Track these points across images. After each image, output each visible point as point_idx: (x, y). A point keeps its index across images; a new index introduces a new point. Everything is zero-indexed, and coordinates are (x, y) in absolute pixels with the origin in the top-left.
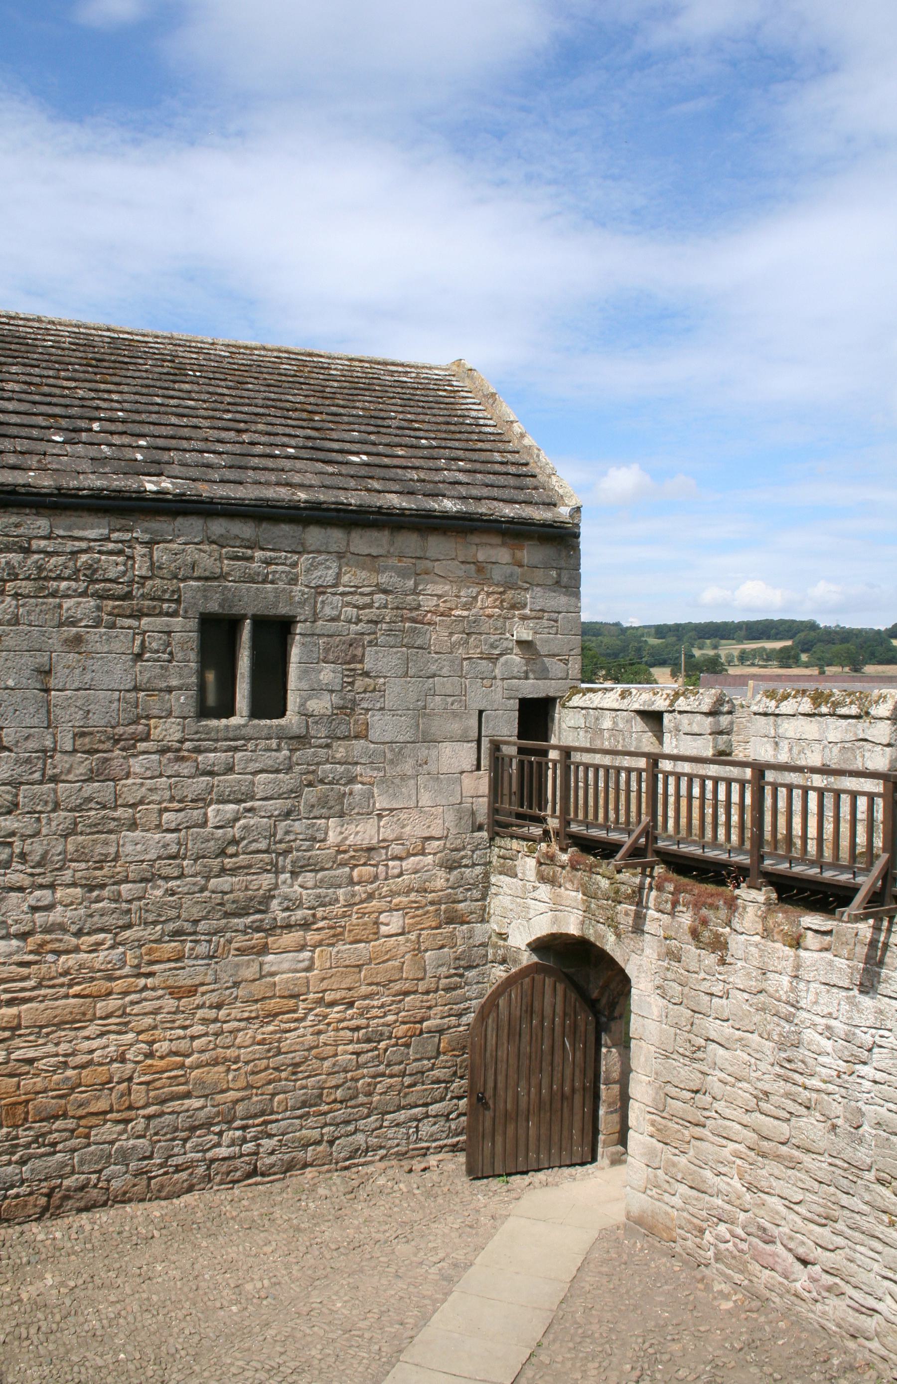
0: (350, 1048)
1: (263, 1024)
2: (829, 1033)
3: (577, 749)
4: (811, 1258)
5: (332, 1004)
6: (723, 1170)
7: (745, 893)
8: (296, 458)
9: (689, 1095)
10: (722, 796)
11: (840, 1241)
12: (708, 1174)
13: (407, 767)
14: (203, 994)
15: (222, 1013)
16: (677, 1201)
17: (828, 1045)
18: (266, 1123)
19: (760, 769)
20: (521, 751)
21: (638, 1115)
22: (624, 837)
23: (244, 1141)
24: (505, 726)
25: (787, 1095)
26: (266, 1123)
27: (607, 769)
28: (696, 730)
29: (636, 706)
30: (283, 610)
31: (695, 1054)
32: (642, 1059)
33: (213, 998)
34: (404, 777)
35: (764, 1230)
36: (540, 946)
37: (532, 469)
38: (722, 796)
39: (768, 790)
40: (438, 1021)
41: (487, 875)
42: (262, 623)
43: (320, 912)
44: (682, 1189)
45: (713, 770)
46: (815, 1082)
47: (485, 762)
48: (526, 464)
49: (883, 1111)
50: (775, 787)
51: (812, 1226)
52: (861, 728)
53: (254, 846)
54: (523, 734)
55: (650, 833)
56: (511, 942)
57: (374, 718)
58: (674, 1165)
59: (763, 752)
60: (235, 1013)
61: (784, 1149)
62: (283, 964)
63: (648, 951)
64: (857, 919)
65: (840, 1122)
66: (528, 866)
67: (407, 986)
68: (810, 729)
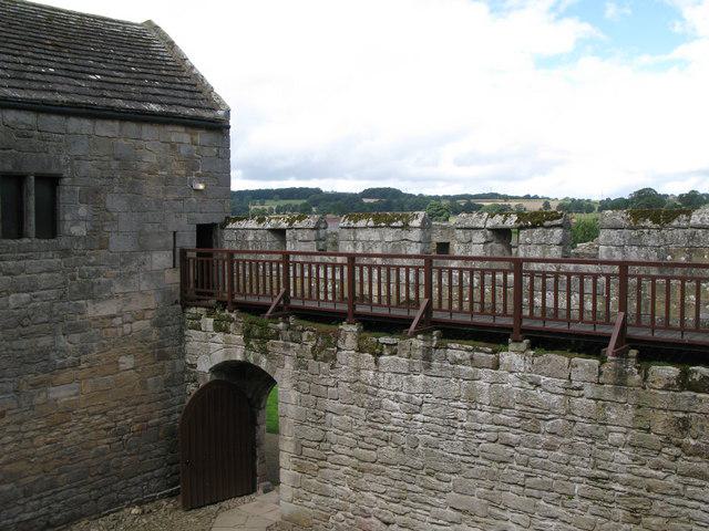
0: (105, 441)
1: (51, 431)
2: (397, 399)
3: (237, 252)
4: (392, 520)
5: (94, 414)
6: (339, 482)
7: (345, 327)
8: (55, 75)
9: (316, 444)
10: (322, 275)
11: (407, 509)
12: (330, 486)
13: (133, 267)
14: (10, 415)
15: (23, 428)
16: (311, 504)
17: (397, 405)
18: (55, 493)
19: (352, 258)
20: (199, 255)
21: (286, 461)
22: (268, 301)
23: (41, 507)
24: (189, 240)
25: (374, 436)
26: (55, 493)
27: (250, 262)
28: (306, 238)
29: (269, 226)
30: (54, 170)
31: (319, 420)
32: (287, 427)
33: (18, 418)
34: (131, 273)
35: (364, 511)
36: (216, 369)
37: (199, 88)
38: (322, 275)
39: (357, 269)
40: (157, 420)
41: (181, 331)
42: (40, 178)
43: (83, 358)
44: (315, 497)
45: (317, 259)
46: (391, 427)
47: (178, 262)
48: (195, 85)
49: (429, 437)
50: (440, 270)
51: (391, 504)
52: (404, 234)
53: (40, 319)
54: (199, 244)
55: (286, 296)
56: (199, 368)
57: (113, 238)
58: (309, 484)
59: (349, 249)
60: (33, 426)
61: (373, 466)
62: (62, 394)
63: (287, 365)
64: (414, 335)
65: (405, 446)
66: (208, 323)
67: (137, 401)
68: (375, 235)
